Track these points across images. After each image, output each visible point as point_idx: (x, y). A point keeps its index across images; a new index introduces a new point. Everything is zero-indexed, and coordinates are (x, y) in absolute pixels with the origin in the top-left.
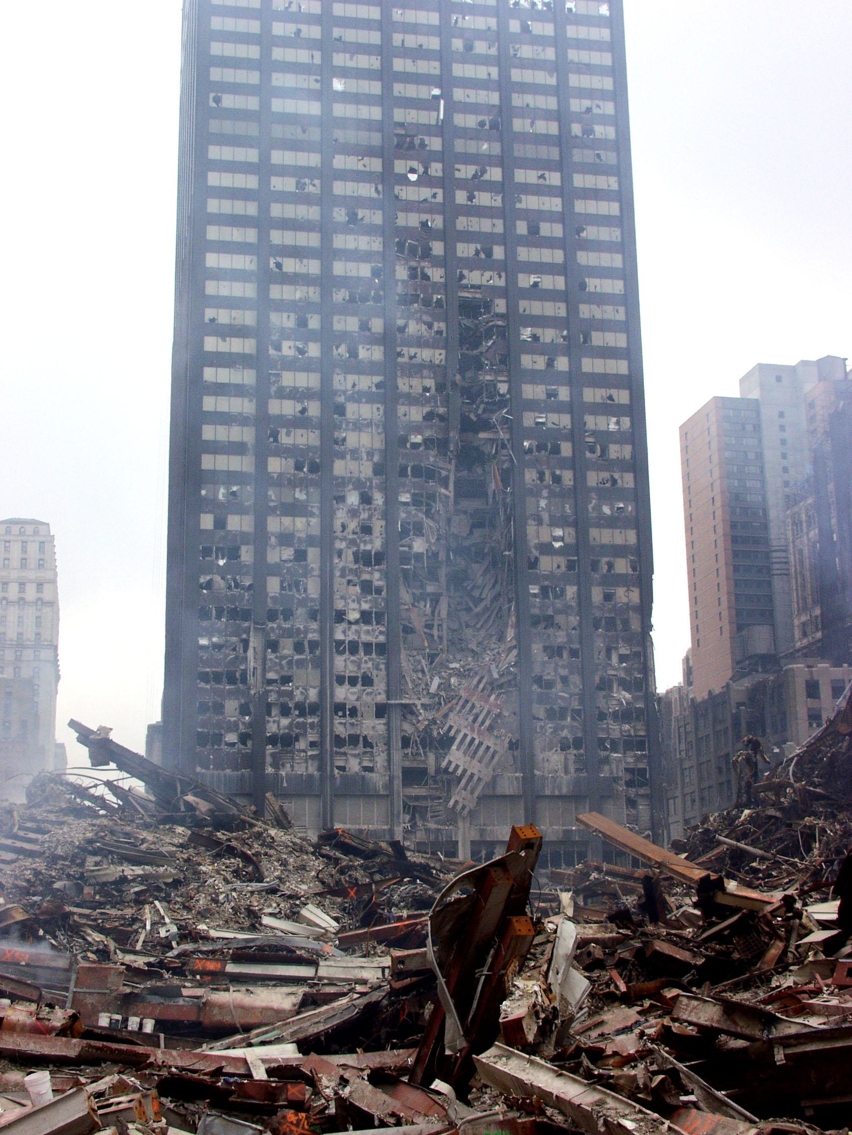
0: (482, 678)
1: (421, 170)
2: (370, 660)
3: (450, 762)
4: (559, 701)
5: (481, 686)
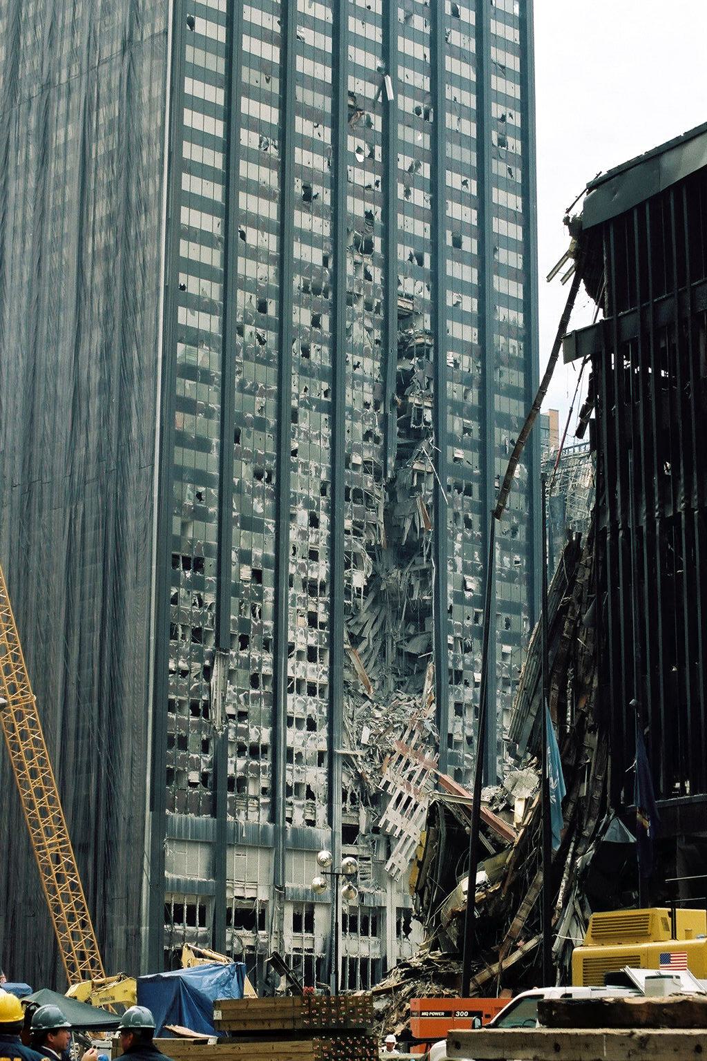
0: (413, 732)
1: (368, 152)
2: (315, 701)
3: (387, 822)
4: (465, 763)
5: (414, 742)
